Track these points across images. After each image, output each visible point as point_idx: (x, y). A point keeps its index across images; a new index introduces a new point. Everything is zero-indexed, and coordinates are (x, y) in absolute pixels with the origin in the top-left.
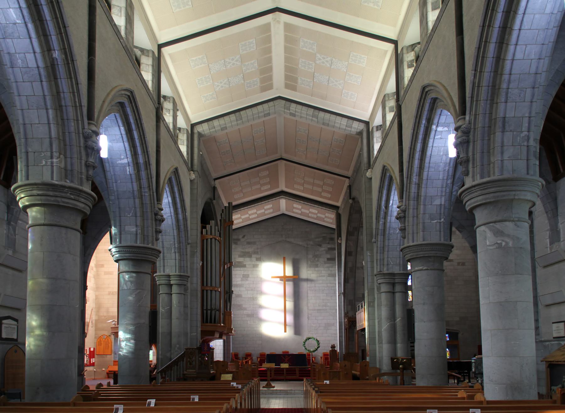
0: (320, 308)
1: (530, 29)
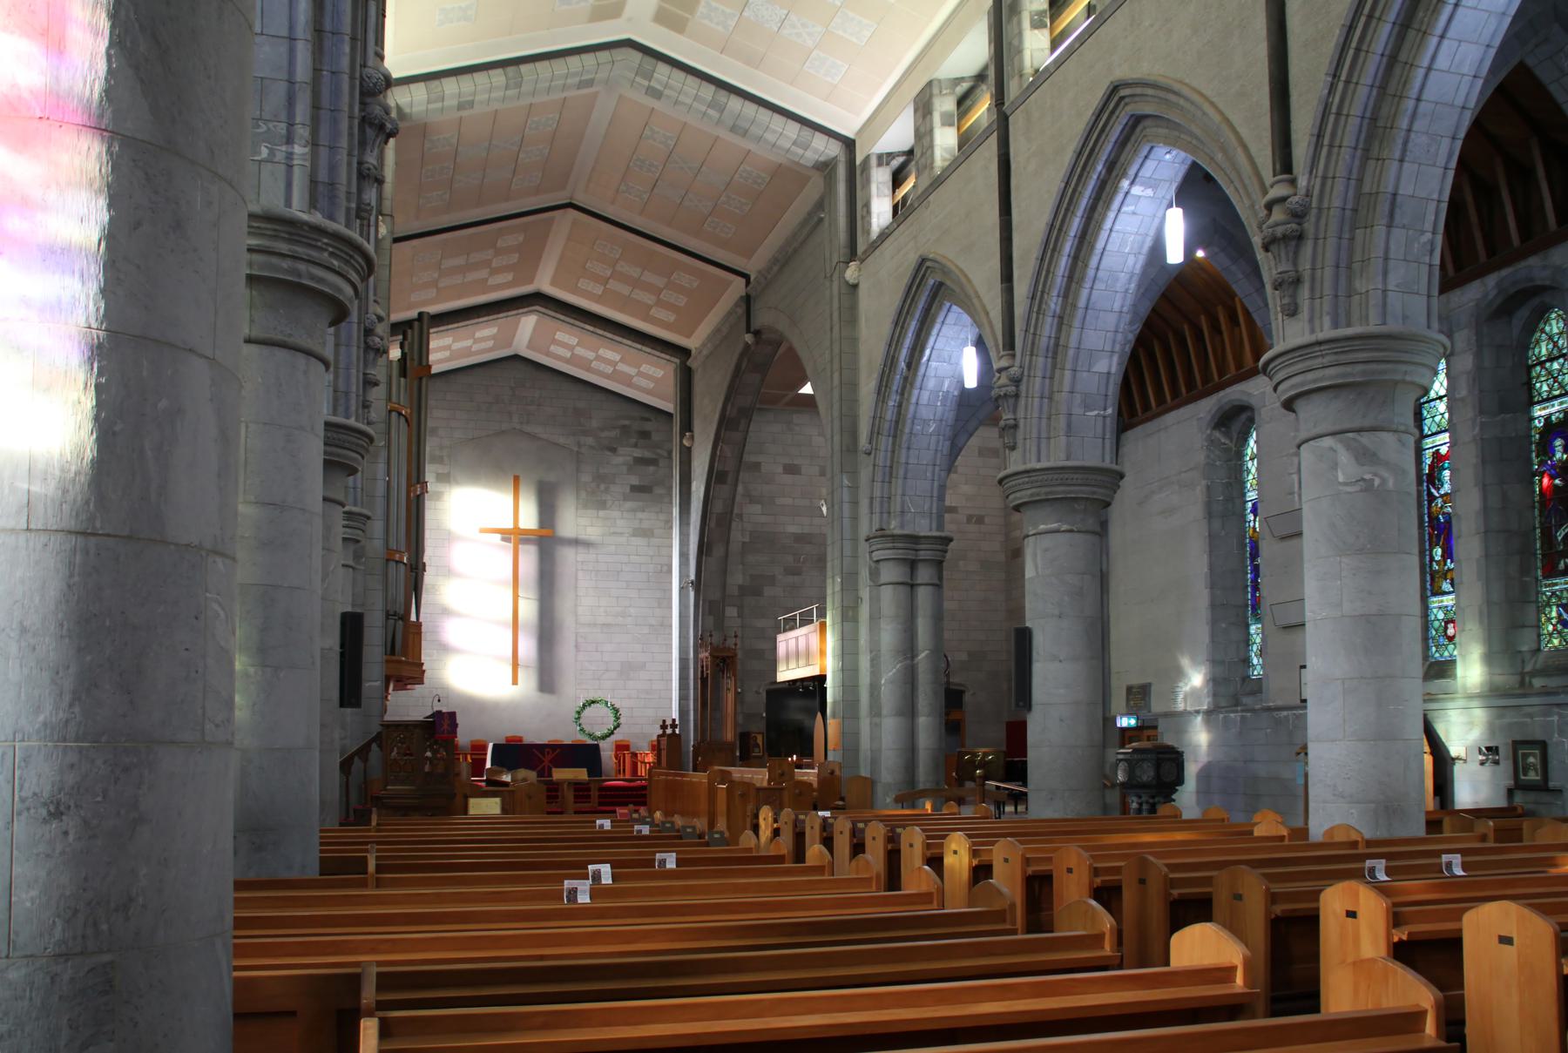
0: (610, 620)
1: (1475, 8)
